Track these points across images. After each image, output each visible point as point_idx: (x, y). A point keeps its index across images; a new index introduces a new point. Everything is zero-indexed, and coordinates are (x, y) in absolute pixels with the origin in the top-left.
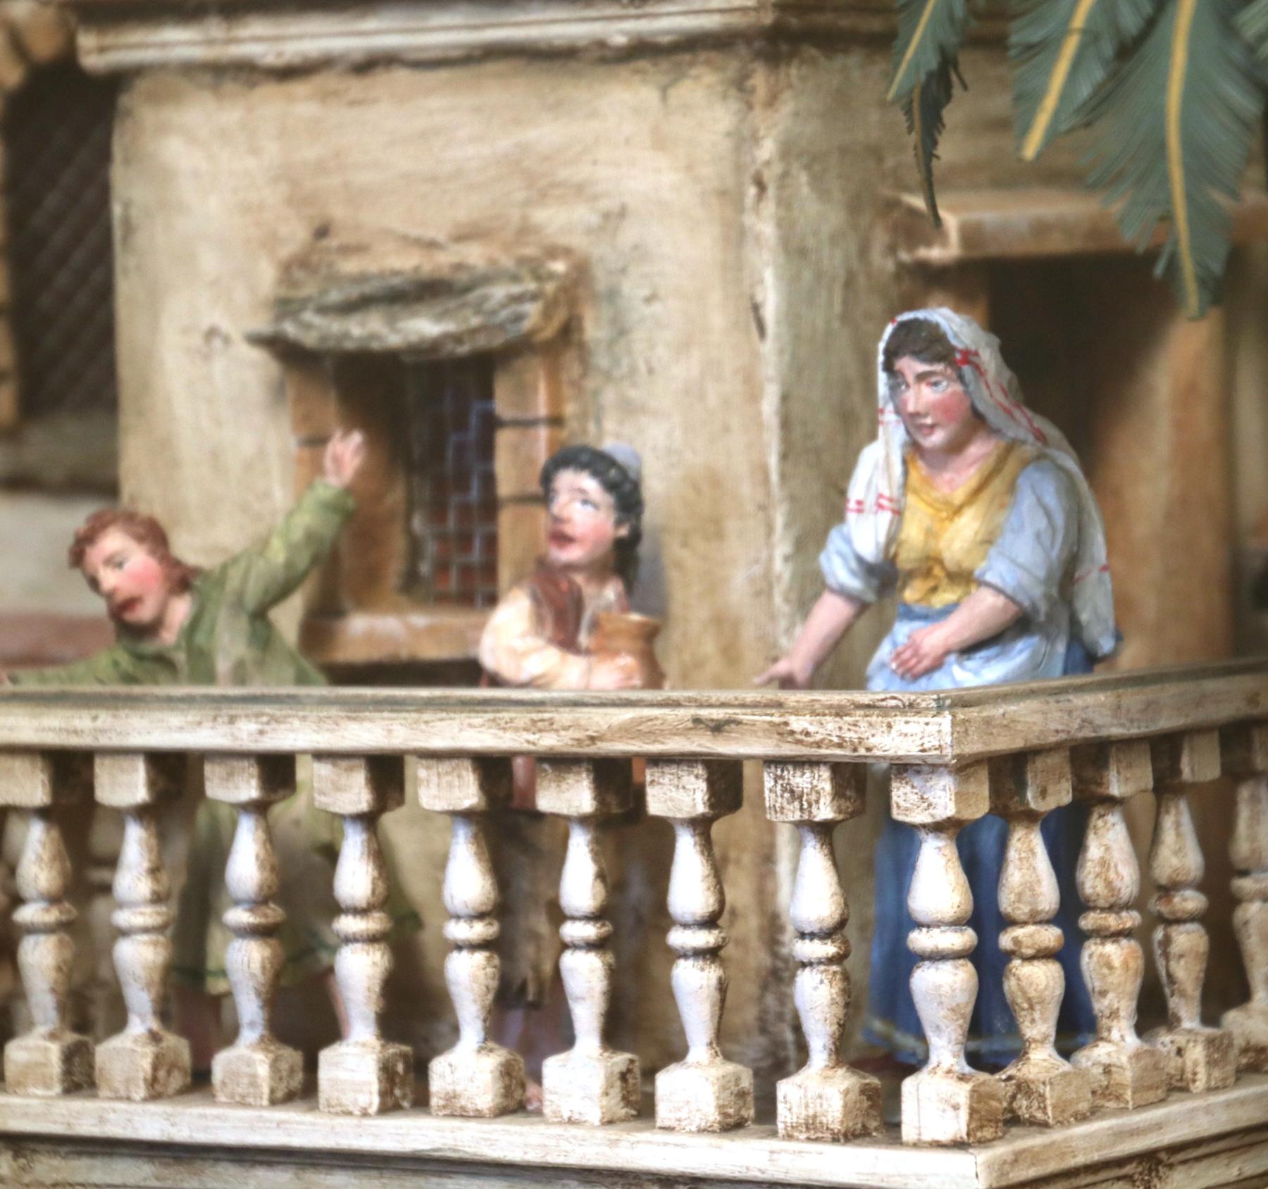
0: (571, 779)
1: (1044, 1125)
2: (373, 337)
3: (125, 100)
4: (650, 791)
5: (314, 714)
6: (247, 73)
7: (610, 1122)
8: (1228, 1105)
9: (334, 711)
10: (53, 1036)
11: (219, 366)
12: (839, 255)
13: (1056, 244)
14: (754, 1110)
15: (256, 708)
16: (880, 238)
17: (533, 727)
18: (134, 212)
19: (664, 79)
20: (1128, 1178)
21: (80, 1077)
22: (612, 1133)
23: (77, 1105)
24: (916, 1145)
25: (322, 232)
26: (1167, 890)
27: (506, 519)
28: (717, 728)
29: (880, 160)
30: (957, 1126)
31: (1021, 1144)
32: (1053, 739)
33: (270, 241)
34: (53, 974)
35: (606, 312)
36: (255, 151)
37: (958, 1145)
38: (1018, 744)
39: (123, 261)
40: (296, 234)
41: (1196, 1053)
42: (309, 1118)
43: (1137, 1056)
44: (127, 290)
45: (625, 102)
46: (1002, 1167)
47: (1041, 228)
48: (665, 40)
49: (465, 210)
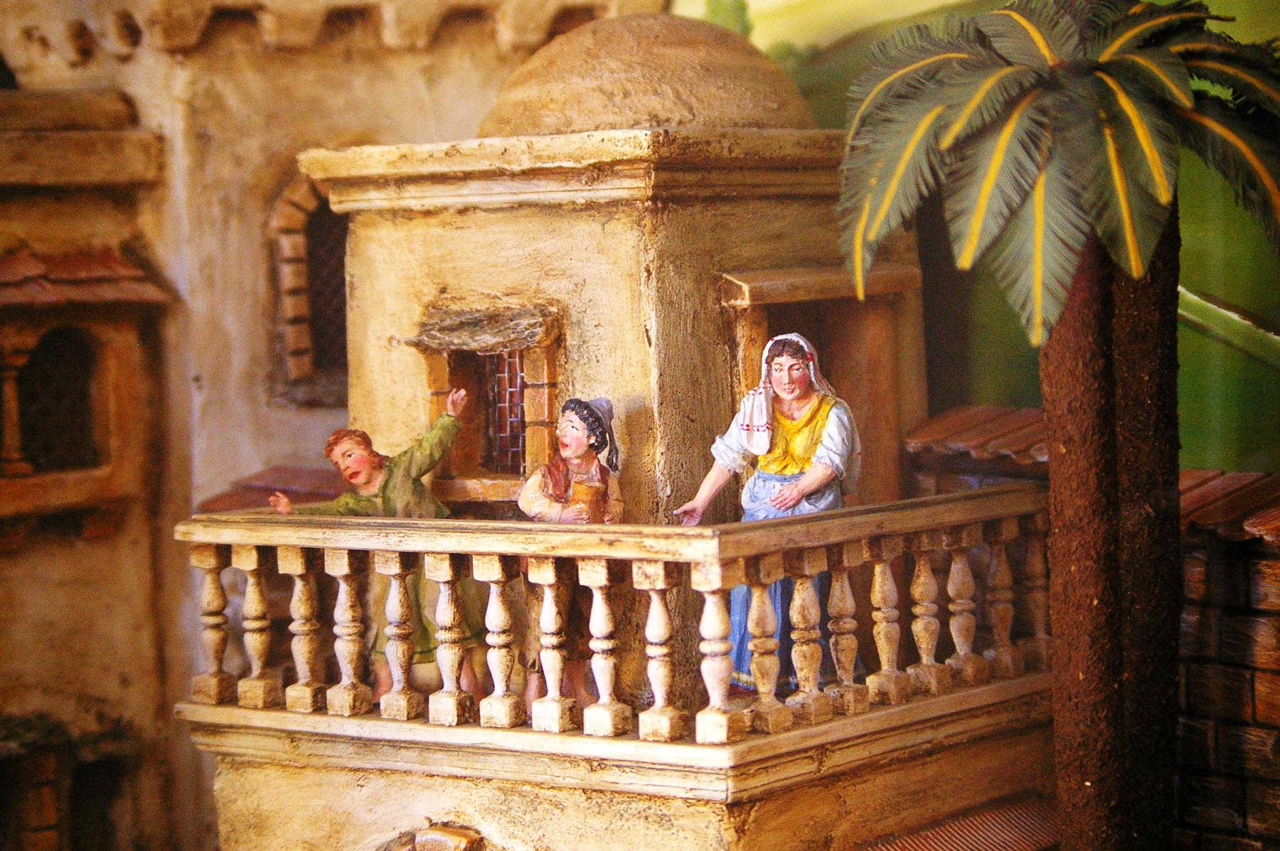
0: (544, 566)
1: (768, 733)
2: (464, 344)
3: (351, 225)
4: (581, 574)
5: (424, 534)
6: (408, 214)
7: (563, 731)
8: (863, 721)
9: (434, 532)
10: (308, 685)
11: (395, 354)
12: (689, 304)
13: (802, 296)
14: (626, 729)
15: (399, 530)
16: (712, 295)
17: (526, 541)
18: (355, 279)
19: (603, 220)
20: (811, 757)
21: (320, 706)
22: (563, 738)
23: (318, 718)
24: (703, 745)
25: (443, 291)
26: (839, 618)
27: (528, 432)
28: (611, 543)
29: (712, 257)
30: (722, 735)
31: (751, 743)
32: (773, 549)
33: (418, 296)
34: (307, 655)
35: (577, 332)
36: (411, 251)
37: (723, 744)
38: (754, 552)
39: (350, 303)
40: (430, 293)
41: (850, 697)
42: (424, 727)
43: (817, 699)
44: (352, 317)
45: (585, 228)
46: (741, 755)
47: (795, 288)
48: (603, 201)
49: (510, 280)
